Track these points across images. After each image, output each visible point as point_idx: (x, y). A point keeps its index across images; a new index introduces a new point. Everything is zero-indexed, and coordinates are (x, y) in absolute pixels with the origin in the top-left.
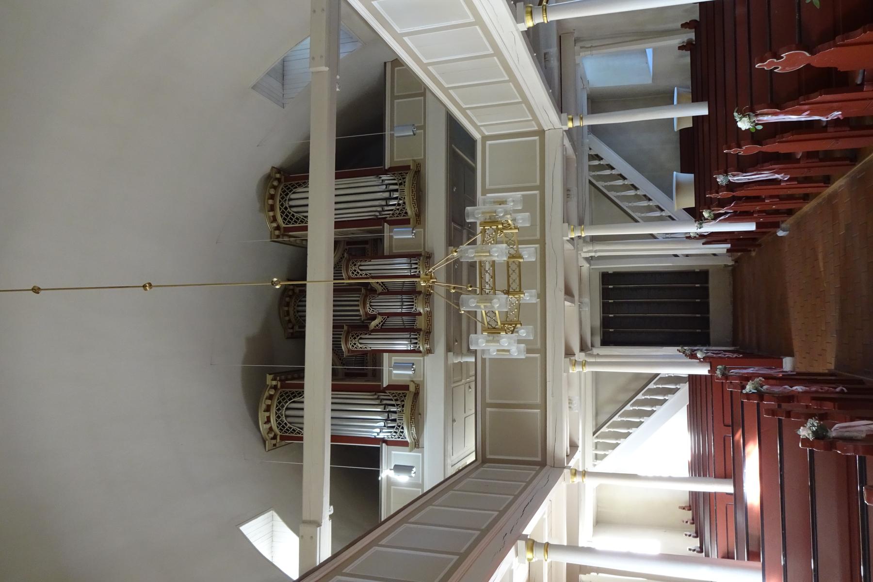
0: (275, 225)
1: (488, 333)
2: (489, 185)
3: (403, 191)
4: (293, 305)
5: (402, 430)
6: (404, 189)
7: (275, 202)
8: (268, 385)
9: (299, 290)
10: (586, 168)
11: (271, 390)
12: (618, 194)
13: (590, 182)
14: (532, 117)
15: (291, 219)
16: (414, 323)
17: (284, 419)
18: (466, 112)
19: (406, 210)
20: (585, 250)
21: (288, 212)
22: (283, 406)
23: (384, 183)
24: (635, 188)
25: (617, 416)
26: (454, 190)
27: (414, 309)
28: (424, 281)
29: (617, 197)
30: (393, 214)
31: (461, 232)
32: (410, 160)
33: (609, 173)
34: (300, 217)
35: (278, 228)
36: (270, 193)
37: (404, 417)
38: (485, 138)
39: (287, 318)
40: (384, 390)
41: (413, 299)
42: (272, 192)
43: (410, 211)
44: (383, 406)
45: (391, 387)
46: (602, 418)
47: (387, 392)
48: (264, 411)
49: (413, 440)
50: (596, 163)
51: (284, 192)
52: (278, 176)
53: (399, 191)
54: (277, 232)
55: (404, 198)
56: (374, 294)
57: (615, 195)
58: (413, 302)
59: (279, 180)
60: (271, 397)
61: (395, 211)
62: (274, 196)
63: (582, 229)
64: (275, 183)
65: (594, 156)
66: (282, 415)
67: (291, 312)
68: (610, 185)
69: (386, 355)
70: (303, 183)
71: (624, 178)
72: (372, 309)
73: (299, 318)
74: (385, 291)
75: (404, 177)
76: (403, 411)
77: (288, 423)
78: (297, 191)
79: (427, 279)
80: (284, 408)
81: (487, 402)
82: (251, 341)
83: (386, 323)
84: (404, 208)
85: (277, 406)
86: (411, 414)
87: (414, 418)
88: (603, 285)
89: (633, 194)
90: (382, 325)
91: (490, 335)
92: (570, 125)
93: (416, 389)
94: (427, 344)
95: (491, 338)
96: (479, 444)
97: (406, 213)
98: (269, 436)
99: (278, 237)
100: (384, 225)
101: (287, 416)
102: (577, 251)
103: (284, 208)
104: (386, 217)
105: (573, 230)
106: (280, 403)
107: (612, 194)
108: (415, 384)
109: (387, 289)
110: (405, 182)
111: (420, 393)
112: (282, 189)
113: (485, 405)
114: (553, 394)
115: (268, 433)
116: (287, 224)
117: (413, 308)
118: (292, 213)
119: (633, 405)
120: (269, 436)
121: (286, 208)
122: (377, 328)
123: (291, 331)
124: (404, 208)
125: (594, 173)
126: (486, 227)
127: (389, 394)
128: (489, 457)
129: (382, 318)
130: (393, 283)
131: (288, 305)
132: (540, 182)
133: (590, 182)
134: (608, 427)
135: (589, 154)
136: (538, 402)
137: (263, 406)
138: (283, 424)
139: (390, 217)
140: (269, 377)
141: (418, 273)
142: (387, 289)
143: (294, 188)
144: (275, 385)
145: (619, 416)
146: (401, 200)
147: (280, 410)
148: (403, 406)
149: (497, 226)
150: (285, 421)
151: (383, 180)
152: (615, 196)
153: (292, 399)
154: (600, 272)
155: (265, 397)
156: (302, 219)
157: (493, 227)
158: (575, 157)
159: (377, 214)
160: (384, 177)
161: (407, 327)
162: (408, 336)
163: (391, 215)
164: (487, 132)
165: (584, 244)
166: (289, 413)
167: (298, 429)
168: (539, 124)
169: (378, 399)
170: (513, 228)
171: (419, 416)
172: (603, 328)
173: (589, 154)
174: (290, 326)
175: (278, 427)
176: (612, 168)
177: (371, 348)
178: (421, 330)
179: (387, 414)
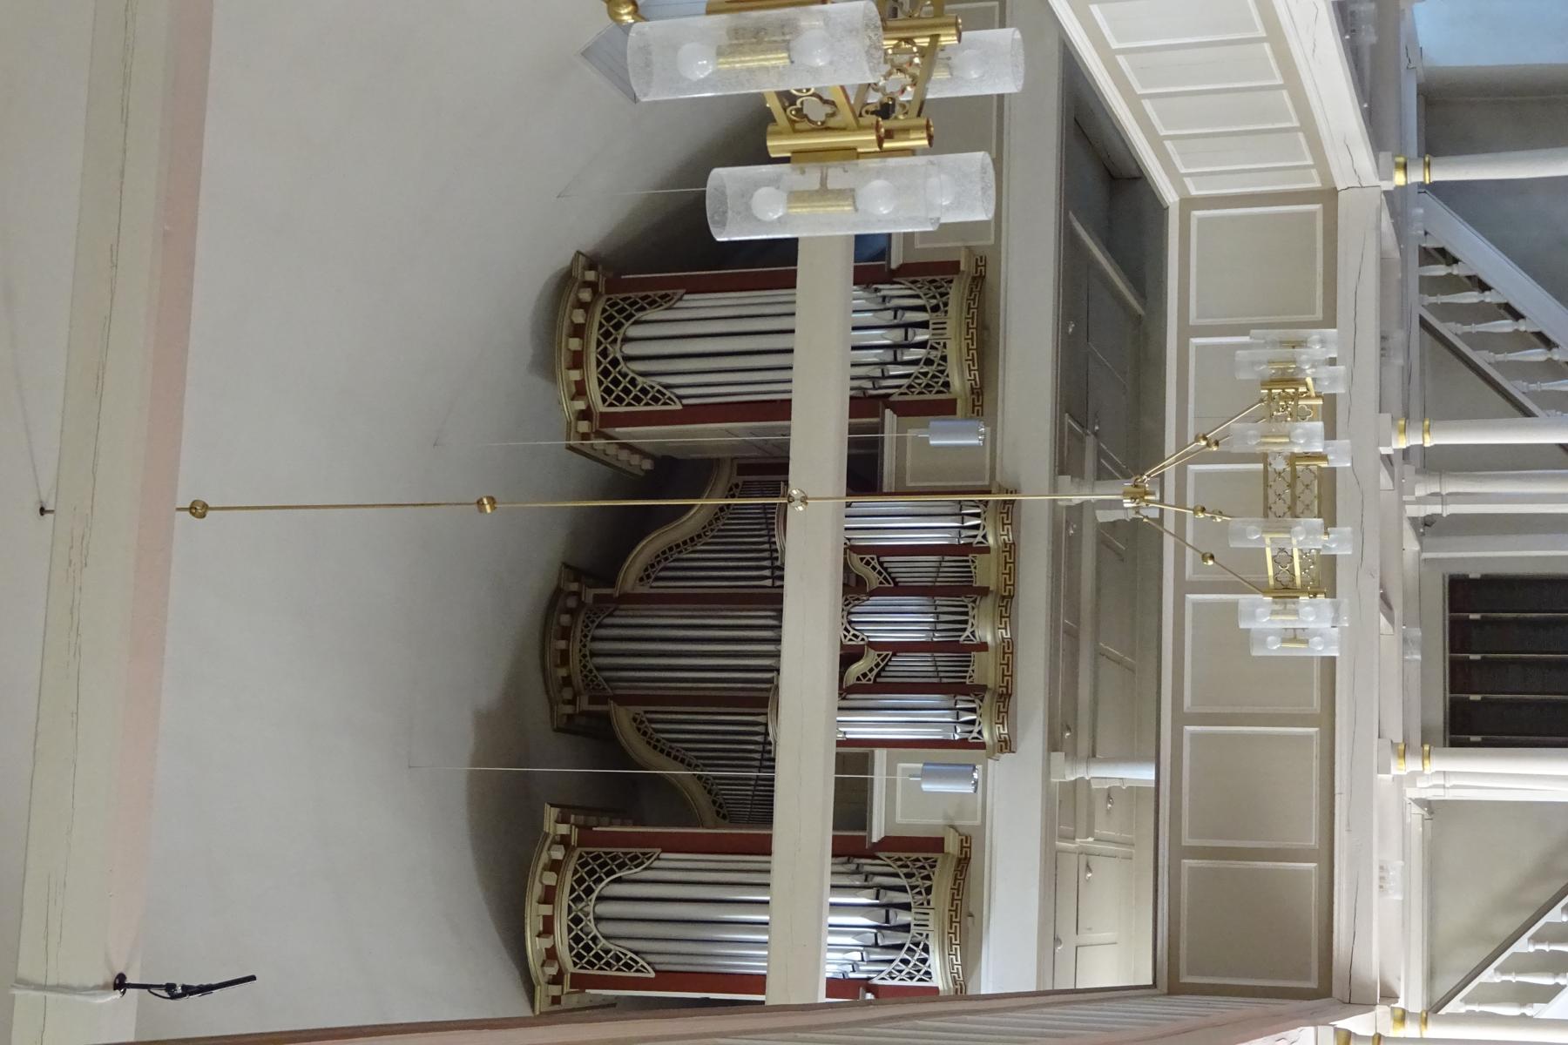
0: (580, 405)
1: (1274, 597)
2: (1198, 317)
3: (941, 326)
4: (579, 634)
5: (925, 955)
6: (945, 323)
7: (585, 345)
8: (547, 835)
9: (596, 596)
10: (1414, 284)
11: (555, 846)
12: (1500, 357)
13: (1424, 323)
14: (1314, 159)
15: (627, 391)
16: (967, 672)
17: (592, 925)
18: (1163, 145)
19: (948, 376)
20: (1421, 491)
21: (620, 372)
22: (589, 891)
23: (888, 305)
24: (1546, 342)
25: (1490, 970)
26: (1070, 330)
27: (967, 633)
28: (1132, 498)
29: (1498, 365)
30: (910, 387)
31: (1081, 440)
32: (959, 248)
33: (1475, 300)
34: (652, 387)
35: (585, 415)
36: (572, 322)
37: (930, 923)
38: (1189, 203)
39: (562, 672)
40: (872, 852)
41: (966, 606)
42: (579, 316)
43: (959, 381)
44: (873, 891)
45: (889, 843)
46: (1444, 985)
47: (880, 854)
48: (539, 903)
49: (951, 985)
50: (1440, 270)
51: (609, 318)
52: (591, 276)
53: (931, 326)
54: (584, 426)
55: (945, 346)
56: (858, 593)
57: (1492, 361)
58: (966, 614)
59: (592, 285)
60: (555, 866)
61: (917, 377)
62: (584, 329)
63: (1426, 428)
64: (586, 295)
65: (1434, 253)
66: (587, 915)
67: (575, 658)
68: (1478, 333)
69: (880, 755)
70: (662, 297)
71: (1517, 316)
72: (852, 632)
73: (595, 672)
74: (887, 585)
75: (942, 290)
76: (929, 903)
77: (603, 937)
78: (643, 319)
79: (1139, 493)
80: (594, 896)
81: (1183, 844)
82: (486, 722)
83: (887, 669)
84: (942, 372)
85: (573, 890)
86: (950, 910)
87: (959, 922)
88: (1452, 610)
89: (1542, 358)
90: (878, 675)
91: (1277, 600)
92: (1399, 179)
93: (962, 847)
94: (1003, 723)
95: (1277, 607)
96: (1162, 950)
97: (946, 385)
98: (543, 972)
99: (585, 436)
100: (883, 413)
101: (598, 919)
102: (1401, 494)
103: (610, 363)
104: (890, 395)
105: (1404, 431)
106: (580, 881)
107: (1481, 358)
108: (960, 835)
109: (893, 579)
110: (946, 304)
111: (972, 860)
112: (604, 311)
113: (1179, 852)
114: (1348, 825)
115: (543, 965)
116: (611, 405)
117: (964, 630)
118: (631, 375)
119: (1536, 939)
120: (543, 972)
121: (615, 363)
122: (864, 681)
123: (568, 709)
124: (942, 372)
125: (1433, 299)
126: (1273, 391)
127: (889, 862)
128: (1186, 979)
129: (879, 655)
130: (917, 564)
131: (565, 634)
132: (1324, 312)
133: (1424, 323)
134: (1466, 1001)
135: (1420, 246)
136: (1313, 843)
137: (537, 891)
138: (587, 940)
139: (901, 394)
140: (551, 813)
141: (979, 539)
142: (893, 579)
143: (637, 310)
144: (562, 836)
145: (1496, 970)
146: (936, 349)
147: (582, 900)
148: (929, 890)
149: (1297, 389)
150: (595, 932)
151: (884, 298)
152: (1490, 364)
153: (615, 873)
154: (1444, 577)
155: (541, 865)
156: (659, 391)
157: (1287, 390)
158: (1397, 255)
159: (868, 384)
160: (886, 290)
161: (945, 680)
162: (951, 704)
163: (903, 390)
164: (1197, 189)
165: (1419, 478)
166: (605, 909)
167: (630, 954)
168: (1325, 173)
169: (857, 872)
170: (1313, 395)
171: (970, 918)
172: (1451, 733)
173: (1420, 246)
174: (567, 694)
175: (571, 949)
176: (1483, 287)
177: (845, 733)
178: (984, 688)
179: (883, 912)
